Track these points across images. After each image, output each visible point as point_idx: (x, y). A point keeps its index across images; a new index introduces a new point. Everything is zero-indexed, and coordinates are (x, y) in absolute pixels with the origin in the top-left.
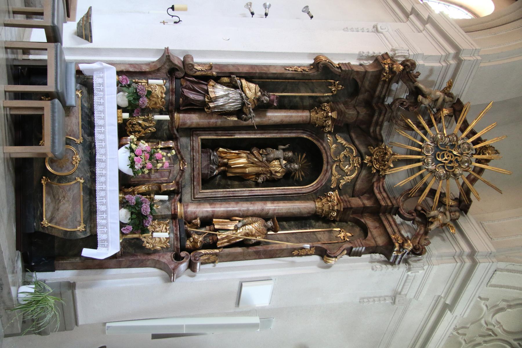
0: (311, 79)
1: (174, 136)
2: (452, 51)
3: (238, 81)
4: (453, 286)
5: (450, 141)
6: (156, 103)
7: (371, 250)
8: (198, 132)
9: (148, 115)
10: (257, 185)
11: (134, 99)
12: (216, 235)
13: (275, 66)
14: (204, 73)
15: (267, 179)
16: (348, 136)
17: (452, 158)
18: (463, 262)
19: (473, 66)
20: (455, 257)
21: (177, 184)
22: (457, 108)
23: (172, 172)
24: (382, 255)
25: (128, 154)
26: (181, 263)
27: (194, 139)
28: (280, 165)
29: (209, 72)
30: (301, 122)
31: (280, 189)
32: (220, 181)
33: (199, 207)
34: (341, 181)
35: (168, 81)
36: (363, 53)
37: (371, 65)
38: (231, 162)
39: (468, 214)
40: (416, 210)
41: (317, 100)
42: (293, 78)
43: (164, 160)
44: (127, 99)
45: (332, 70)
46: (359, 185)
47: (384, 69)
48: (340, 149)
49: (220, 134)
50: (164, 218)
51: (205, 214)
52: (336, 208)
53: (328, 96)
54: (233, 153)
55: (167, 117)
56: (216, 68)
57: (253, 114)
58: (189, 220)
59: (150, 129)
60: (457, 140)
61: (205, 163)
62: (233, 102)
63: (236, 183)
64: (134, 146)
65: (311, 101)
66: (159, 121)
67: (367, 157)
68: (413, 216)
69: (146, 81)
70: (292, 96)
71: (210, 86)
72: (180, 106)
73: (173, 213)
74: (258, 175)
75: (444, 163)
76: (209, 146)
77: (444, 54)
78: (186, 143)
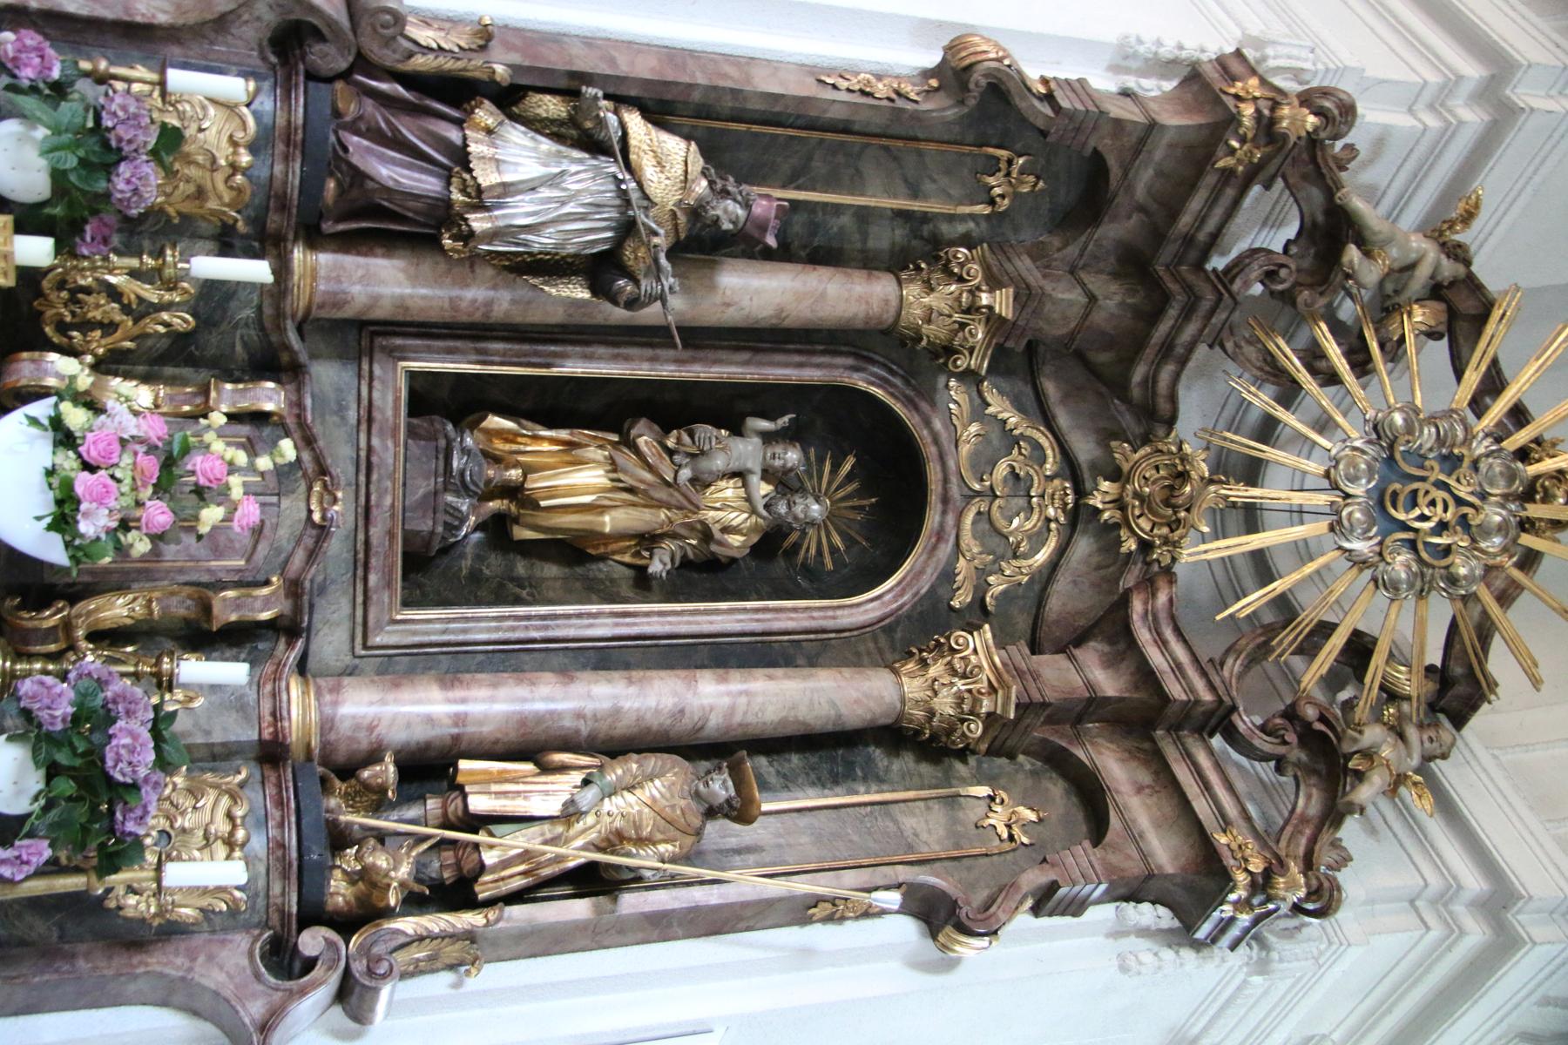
0: (916, 139)
1: (285, 358)
2: (1473, 71)
3: (612, 119)
4: (1389, 1011)
5: (1440, 441)
6: (200, 194)
7: (1122, 891)
8: (399, 341)
9: (160, 254)
10: (643, 585)
11: (83, 163)
12: (476, 846)
13: (773, 65)
14: (449, 65)
15: (684, 556)
16: (1028, 390)
17: (1445, 510)
18: (1455, 931)
19: (1556, 136)
20: (1418, 903)
21: (294, 589)
22: (1467, 305)
23: (267, 531)
24: (1162, 910)
25: (42, 452)
26: (303, 992)
27: (377, 371)
28: (748, 499)
29: (478, 61)
30: (859, 325)
31: (745, 610)
32: (479, 558)
33: (391, 696)
34: (991, 579)
35: (267, 85)
36: (1140, 41)
37: (1166, 98)
38: (536, 483)
39: (1466, 731)
40: (1291, 714)
41: (926, 230)
42: (844, 128)
43: (237, 492)
44: (43, 163)
45: (1022, 105)
46: (1063, 599)
47: (1233, 120)
48: (996, 442)
49: (496, 353)
50: (218, 756)
51: (420, 734)
52: (986, 706)
53: (972, 217)
54: (543, 438)
55: (257, 271)
56: (509, 47)
57: (669, 281)
58: (344, 766)
59: (165, 316)
60: (1467, 441)
61: (422, 487)
62: (582, 218)
63: (551, 570)
64: (76, 418)
65: (900, 234)
66: (214, 291)
67: (1105, 485)
68: (1285, 743)
69: (154, 77)
70: (826, 204)
71: (477, 128)
72: (321, 216)
73: (267, 735)
74: (648, 540)
75: (1416, 531)
76: (442, 405)
77: (1433, 78)
78: (339, 390)
